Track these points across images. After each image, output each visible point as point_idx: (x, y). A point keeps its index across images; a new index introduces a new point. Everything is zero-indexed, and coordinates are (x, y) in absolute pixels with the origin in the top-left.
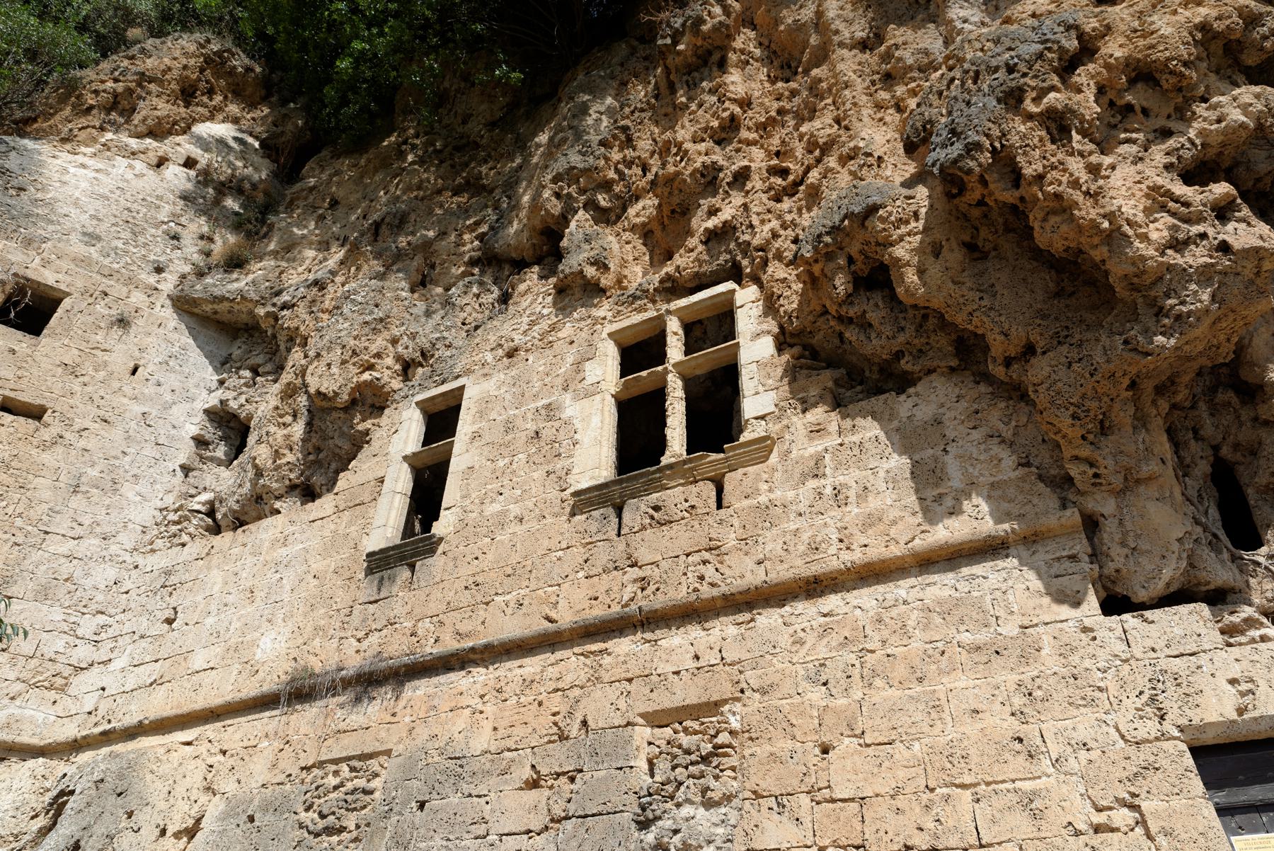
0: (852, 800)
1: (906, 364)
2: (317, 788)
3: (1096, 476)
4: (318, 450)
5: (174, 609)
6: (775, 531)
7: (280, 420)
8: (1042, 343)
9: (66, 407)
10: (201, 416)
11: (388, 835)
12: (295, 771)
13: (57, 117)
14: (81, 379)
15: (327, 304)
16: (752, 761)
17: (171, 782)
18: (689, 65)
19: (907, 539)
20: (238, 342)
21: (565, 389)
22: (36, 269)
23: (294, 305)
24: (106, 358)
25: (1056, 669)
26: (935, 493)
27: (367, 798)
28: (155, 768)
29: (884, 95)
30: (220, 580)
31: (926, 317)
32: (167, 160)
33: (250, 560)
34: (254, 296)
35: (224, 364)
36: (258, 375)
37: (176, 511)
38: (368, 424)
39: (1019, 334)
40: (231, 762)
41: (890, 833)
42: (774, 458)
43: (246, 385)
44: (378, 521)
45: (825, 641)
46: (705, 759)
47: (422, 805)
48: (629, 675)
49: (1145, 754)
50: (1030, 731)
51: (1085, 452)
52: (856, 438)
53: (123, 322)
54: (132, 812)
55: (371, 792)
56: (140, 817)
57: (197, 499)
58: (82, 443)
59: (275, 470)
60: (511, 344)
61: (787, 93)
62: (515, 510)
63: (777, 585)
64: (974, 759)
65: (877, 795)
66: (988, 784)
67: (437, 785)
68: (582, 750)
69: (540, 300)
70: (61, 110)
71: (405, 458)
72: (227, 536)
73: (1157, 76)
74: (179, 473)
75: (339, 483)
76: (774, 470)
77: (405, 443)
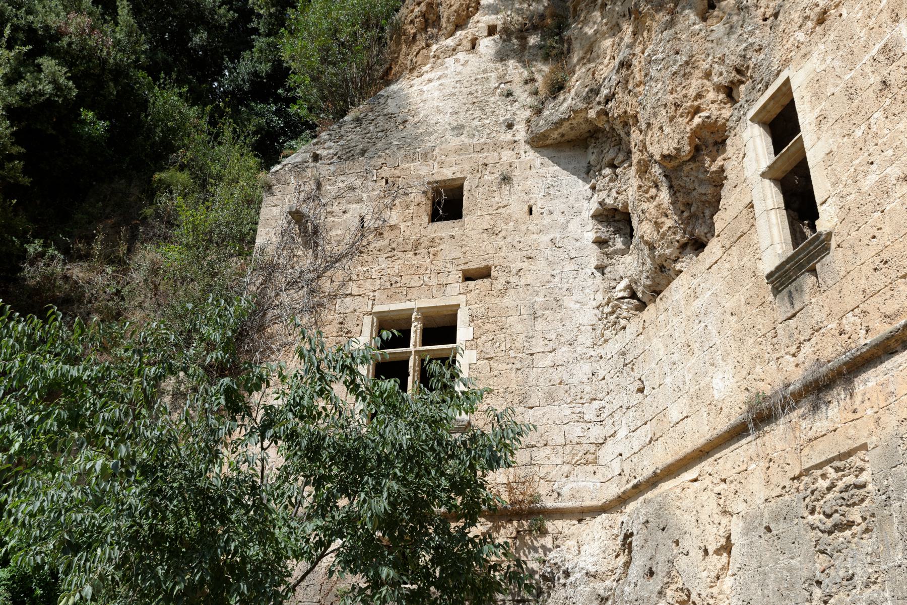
2: (812, 493)
4: (688, 205)
5: (640, 379)
7: (647, 196)
9: (501, 260)
10: (591, 223)
11: (896, 521)
12: (787, 483)
13: (401, 57)
14: (500, 235)
15: (638, 77)
17: (695, 512)
20: (590, 150)
22: (438, 172)
23: (614, 95)
24: (508, 211)
27: (862, 492)
28: (679, 504)
30: (661, 345)
32: (476, 39)
33: (676, 320)
34: (582, 106)
35: (588, 173)
36: (617, 167)
37: (608, 304)
38: (719, 162)
40: (733, 487)
43: (611, 180)
44: (764, 243)
53: (506, 179)
54: (677, 540)
55: (863, 486)
56: (685, 543)
57: (618, 288)
58: (523, 281)
59: (662, 238)
60: (817, 10)
70: (400, 50)
71: (763, 175)
72: (651, 307)
74: (598, 274)
77: (757, 161)
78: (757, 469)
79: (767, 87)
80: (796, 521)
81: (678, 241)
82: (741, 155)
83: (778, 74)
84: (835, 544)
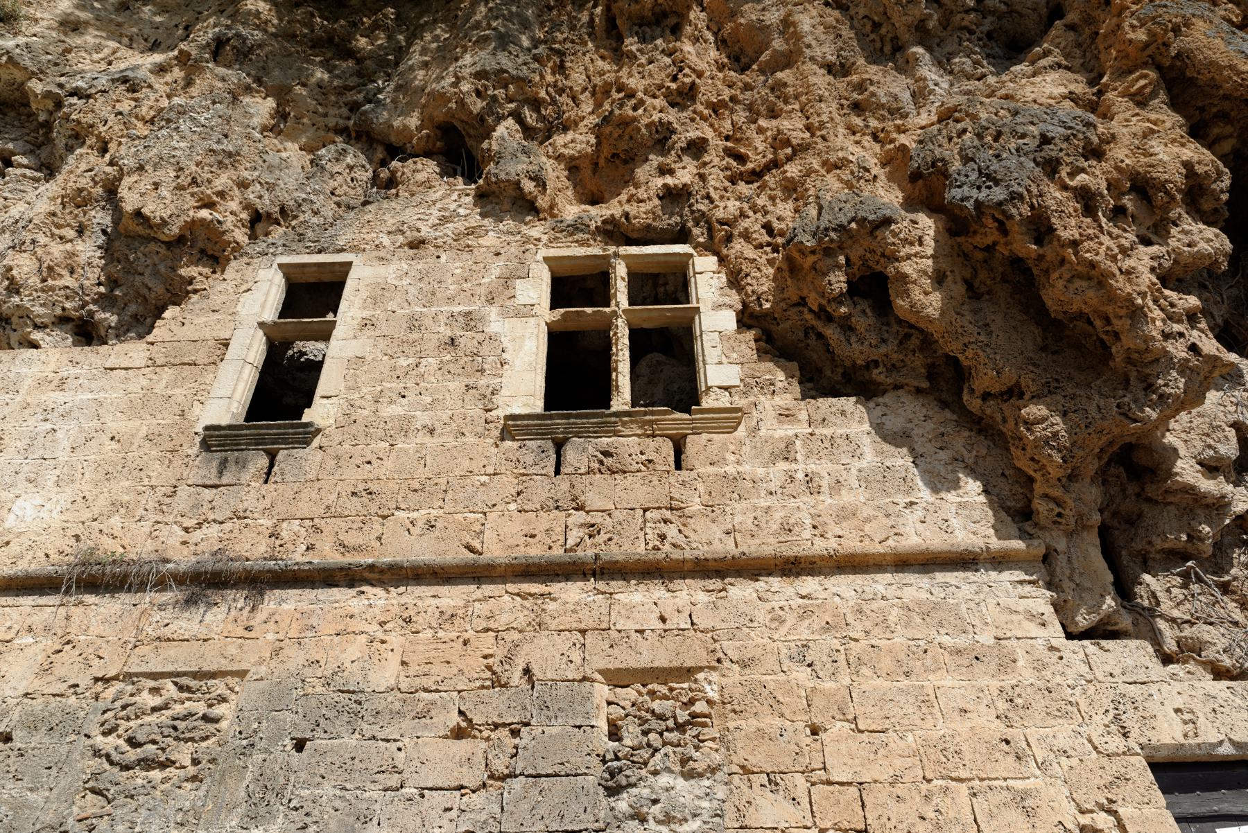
0: (849, 784)
1: (878, 375)
3: (1059, 515)
6: (744, 504)
8: (1033, 388)
11: (249, 776)
12: (84, 681)
16: (737, 734)
18: (643, 18)
19: (882, 538)
21: (491, 301)
23: (89, 97)
25: (1031, 680)
26: (907, 501)
27: (211, 727)
29: (857, 121)
31: (914, 334)
39: (1010, 375)
41: (893, 821)
42: (741, 431)
45: (806, 623)
46: (680, 727)
47: (300, 746)
48: (583, 626)
49: (1115, 767)
50: (1015, 734)
51: (1057, 492)
52: (827, 431)
59: (43, 290)
61: (740, 84)
62: (423, 418)
63: (755, 559)
64: (967, 756)
65: (875, 781)
66: (982, 780)
67: (322, 721)
68: (527, 701)
69: (455, 196)
71: (262, 325)
73: (1151, 192)
75: (155, 331)
76: (742, 444)
77: (263, 306)
78: (35, 649)
79: (320, 252)
80: (73, 737)
81: (64, 309)
82: (244, 288)
83: (342, 250)
84: (130, 785)
